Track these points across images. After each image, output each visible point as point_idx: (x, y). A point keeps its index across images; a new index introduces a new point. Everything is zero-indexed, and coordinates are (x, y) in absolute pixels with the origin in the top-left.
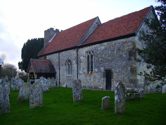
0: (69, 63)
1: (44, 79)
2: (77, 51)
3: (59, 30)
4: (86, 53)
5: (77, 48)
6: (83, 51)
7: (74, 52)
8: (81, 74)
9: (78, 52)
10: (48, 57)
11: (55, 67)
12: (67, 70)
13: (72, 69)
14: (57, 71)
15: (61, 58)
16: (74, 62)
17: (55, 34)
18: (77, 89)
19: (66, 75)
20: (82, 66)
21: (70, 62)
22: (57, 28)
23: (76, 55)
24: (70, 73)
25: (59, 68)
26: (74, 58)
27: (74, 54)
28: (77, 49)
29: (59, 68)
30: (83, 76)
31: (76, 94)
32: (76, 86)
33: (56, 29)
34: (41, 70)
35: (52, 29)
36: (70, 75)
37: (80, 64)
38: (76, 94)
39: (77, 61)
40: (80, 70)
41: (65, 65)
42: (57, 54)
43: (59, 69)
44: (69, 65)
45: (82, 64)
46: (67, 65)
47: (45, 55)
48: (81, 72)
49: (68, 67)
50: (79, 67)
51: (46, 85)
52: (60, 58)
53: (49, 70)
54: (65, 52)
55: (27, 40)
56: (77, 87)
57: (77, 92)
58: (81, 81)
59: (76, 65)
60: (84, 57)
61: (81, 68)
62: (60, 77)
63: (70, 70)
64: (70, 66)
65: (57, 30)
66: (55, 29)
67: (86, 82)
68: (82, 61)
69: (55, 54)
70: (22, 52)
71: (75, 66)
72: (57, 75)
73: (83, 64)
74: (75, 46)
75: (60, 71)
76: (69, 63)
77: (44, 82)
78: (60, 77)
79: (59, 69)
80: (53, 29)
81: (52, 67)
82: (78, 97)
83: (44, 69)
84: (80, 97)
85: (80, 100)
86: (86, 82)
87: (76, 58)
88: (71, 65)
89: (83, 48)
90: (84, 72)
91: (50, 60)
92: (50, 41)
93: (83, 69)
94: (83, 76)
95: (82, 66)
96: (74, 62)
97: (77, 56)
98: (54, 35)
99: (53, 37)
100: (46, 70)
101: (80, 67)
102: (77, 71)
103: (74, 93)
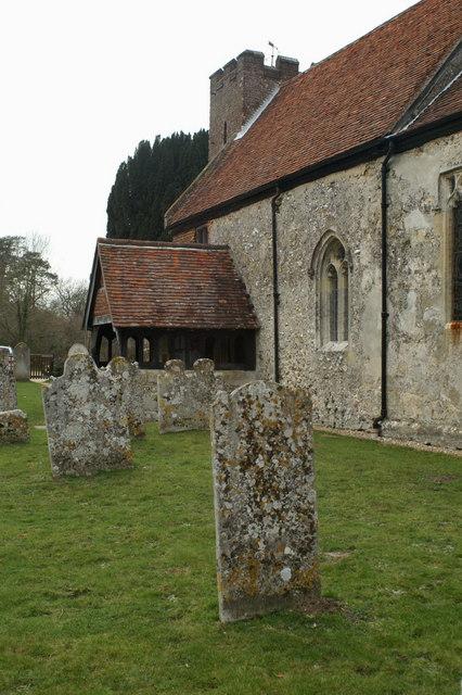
0: (337, 264)
1: (93, 375)
2: (386, 171)
3: (295, 64)
4: (446, 185)
5: (384, 150)
6: (422, 171)
7: (361, 182)
8: (408, 339)
9: (392, 181)
10: (218, 230)
11: (254, 294)
12: (320, 313)
13: (353, 301)
14: (265, 317)
15: (288, 230)
16: (364, 253)
17: (271, 88)
18: (266, 486)
19: (316, 342)
20: (418, 278)
21: (342, 254)
22: (288, 54)
23: (378, 204)
24: (341, 329)
25: (276, 296)
26: (364, 225)
27: (362, 198)
28: (383, 159)
29: (276, 296)
30: (420, 355)
31: (253, 531)
32: (257, 450)
33: (281, 61)
34: (161, 311)
35: (251, 59)
36: (340, 346)
37: (405, 263)
38: (253, 531)
39: (385, 246)
40: (403, 305)
41: (312, 274)
42: (266, 205)
43: (277, 303)
44: (334, 279)
45: (413, 266)
46: (326, 276)
47: (200, 221)
48: (406, 323)
49: (327, 287)
50: (395, 284)
51: (109, 417)
52: (280, 228)
53: (210, 312)
54: (311, 186)
55: (136, 145)
56: (260, 463)
57: (260, 518)
58: (306, 404)
59: (378, 273)
60: (427, 210)
61: (412, 297)
62: (277, 359)
63: (334, 314)
64: (341, 279)
65: (287, 66)
66: (269, 62)
67: (444, 397)
68: (414, 241)
69: (253, 209)
70: (109, 211)
71: (369, 276)
72: (265, 345)
73: (426, 266)
74: (371, 137)
75: (281, 318)
76: (337, 264)
77: (95, 396)
78: (277, 359)
79: (277, 303)
80: (259, 57)
81: (232, 288)
82: (272, 563)
83: (180, 304)
84: (295, 564)
85: (287, 593)
86: (444, 397)
87: (379, 225)
88: (346, 275)
89: (425, 147)
90: (430, 325)
91: (227, 247)
92: (240, 136)
93: (424, 302)
94: (421, 349)
95: (415, 282)
96: (364, 253)
97: (385, 206)
98: (264, 95)
99: (257, 105)
100: (190, 312)
101: (401, 285)
102: (385, 316)
103: (226, 525)
